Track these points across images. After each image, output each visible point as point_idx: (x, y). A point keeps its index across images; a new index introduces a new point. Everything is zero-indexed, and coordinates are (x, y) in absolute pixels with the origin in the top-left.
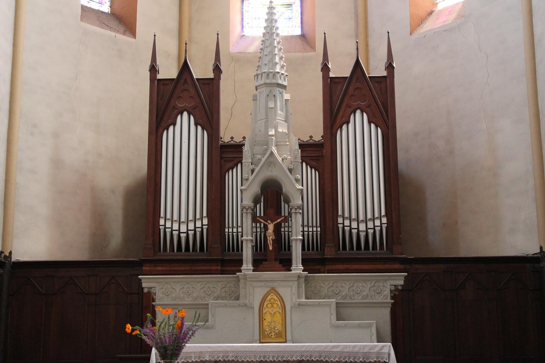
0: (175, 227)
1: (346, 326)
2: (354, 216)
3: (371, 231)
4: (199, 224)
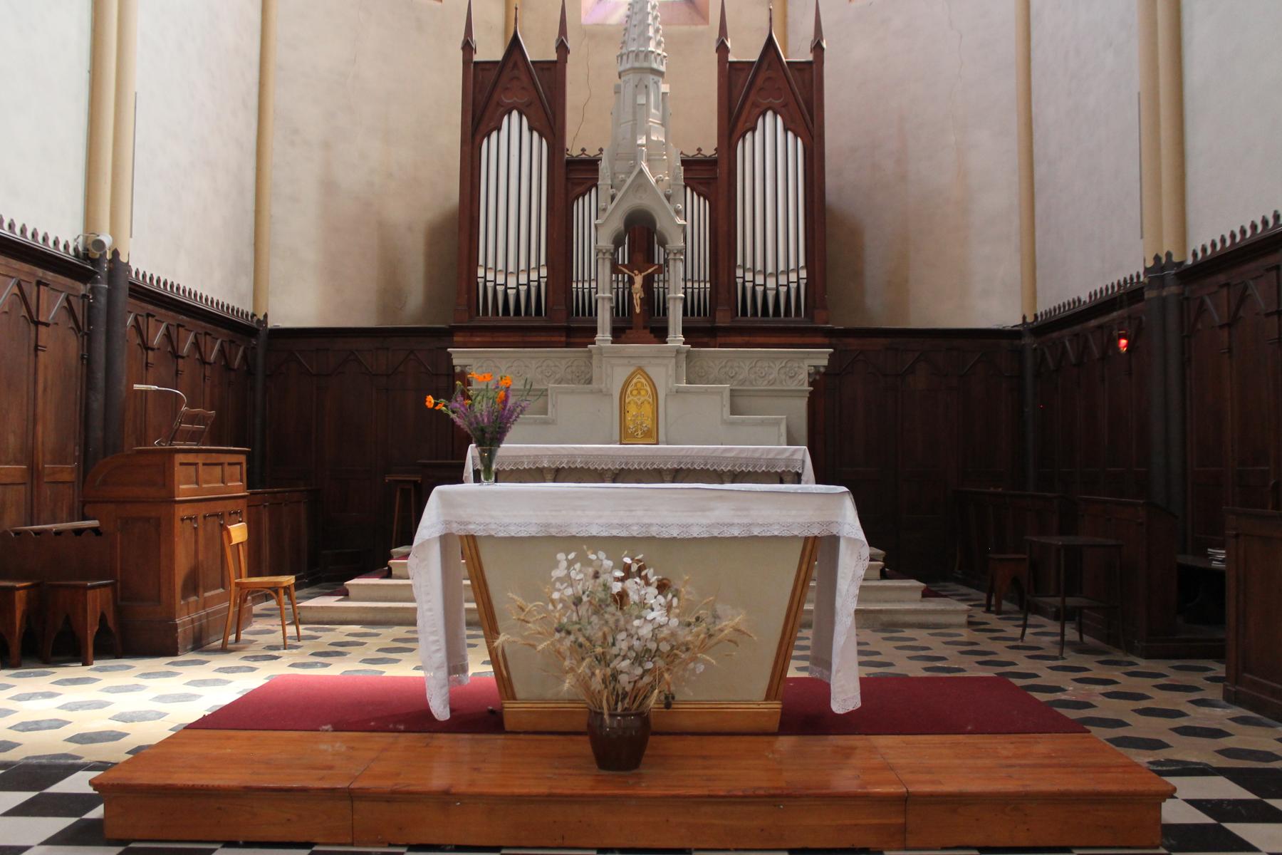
0: (501, 279)
1: (743, 423)
2: (759, 267)
3: (783, 290)
4: (534, 276)
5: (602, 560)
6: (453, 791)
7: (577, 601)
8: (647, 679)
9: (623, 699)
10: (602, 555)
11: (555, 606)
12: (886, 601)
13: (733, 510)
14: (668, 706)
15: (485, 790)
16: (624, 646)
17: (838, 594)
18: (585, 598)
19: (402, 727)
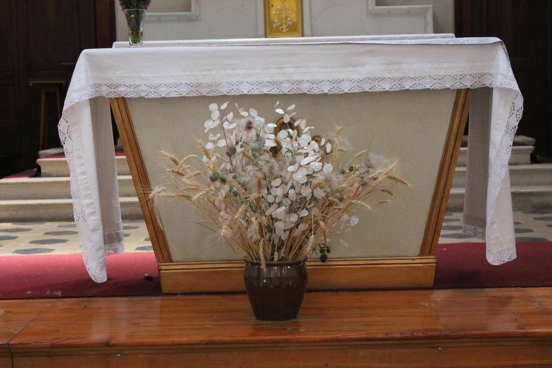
1: (389, 14)
5: (254, 117)
6: (114, 342)
7: (231, 152)
8: (303, 227)
9: (279, 249)
10: (253, 112)
11: (208, 157)
12: (536, 185)
13: (384, 64)
14: (324, 259)
15: (146, 340)
16: (279, 192)
17: (491, 145)
18: (239, 149)
19: (59, 293)
